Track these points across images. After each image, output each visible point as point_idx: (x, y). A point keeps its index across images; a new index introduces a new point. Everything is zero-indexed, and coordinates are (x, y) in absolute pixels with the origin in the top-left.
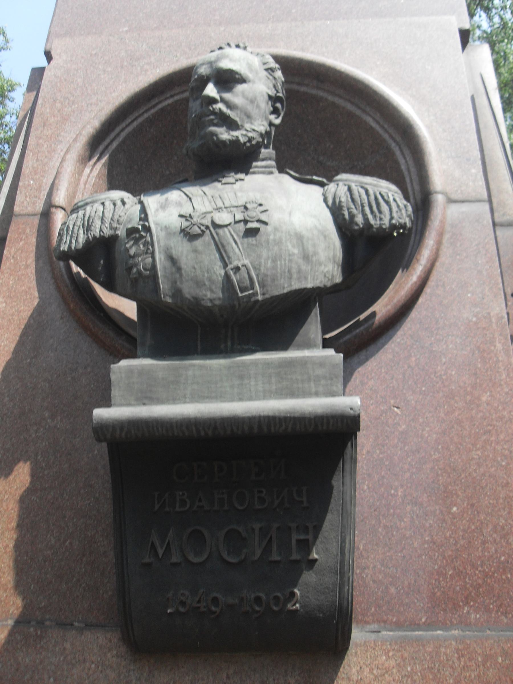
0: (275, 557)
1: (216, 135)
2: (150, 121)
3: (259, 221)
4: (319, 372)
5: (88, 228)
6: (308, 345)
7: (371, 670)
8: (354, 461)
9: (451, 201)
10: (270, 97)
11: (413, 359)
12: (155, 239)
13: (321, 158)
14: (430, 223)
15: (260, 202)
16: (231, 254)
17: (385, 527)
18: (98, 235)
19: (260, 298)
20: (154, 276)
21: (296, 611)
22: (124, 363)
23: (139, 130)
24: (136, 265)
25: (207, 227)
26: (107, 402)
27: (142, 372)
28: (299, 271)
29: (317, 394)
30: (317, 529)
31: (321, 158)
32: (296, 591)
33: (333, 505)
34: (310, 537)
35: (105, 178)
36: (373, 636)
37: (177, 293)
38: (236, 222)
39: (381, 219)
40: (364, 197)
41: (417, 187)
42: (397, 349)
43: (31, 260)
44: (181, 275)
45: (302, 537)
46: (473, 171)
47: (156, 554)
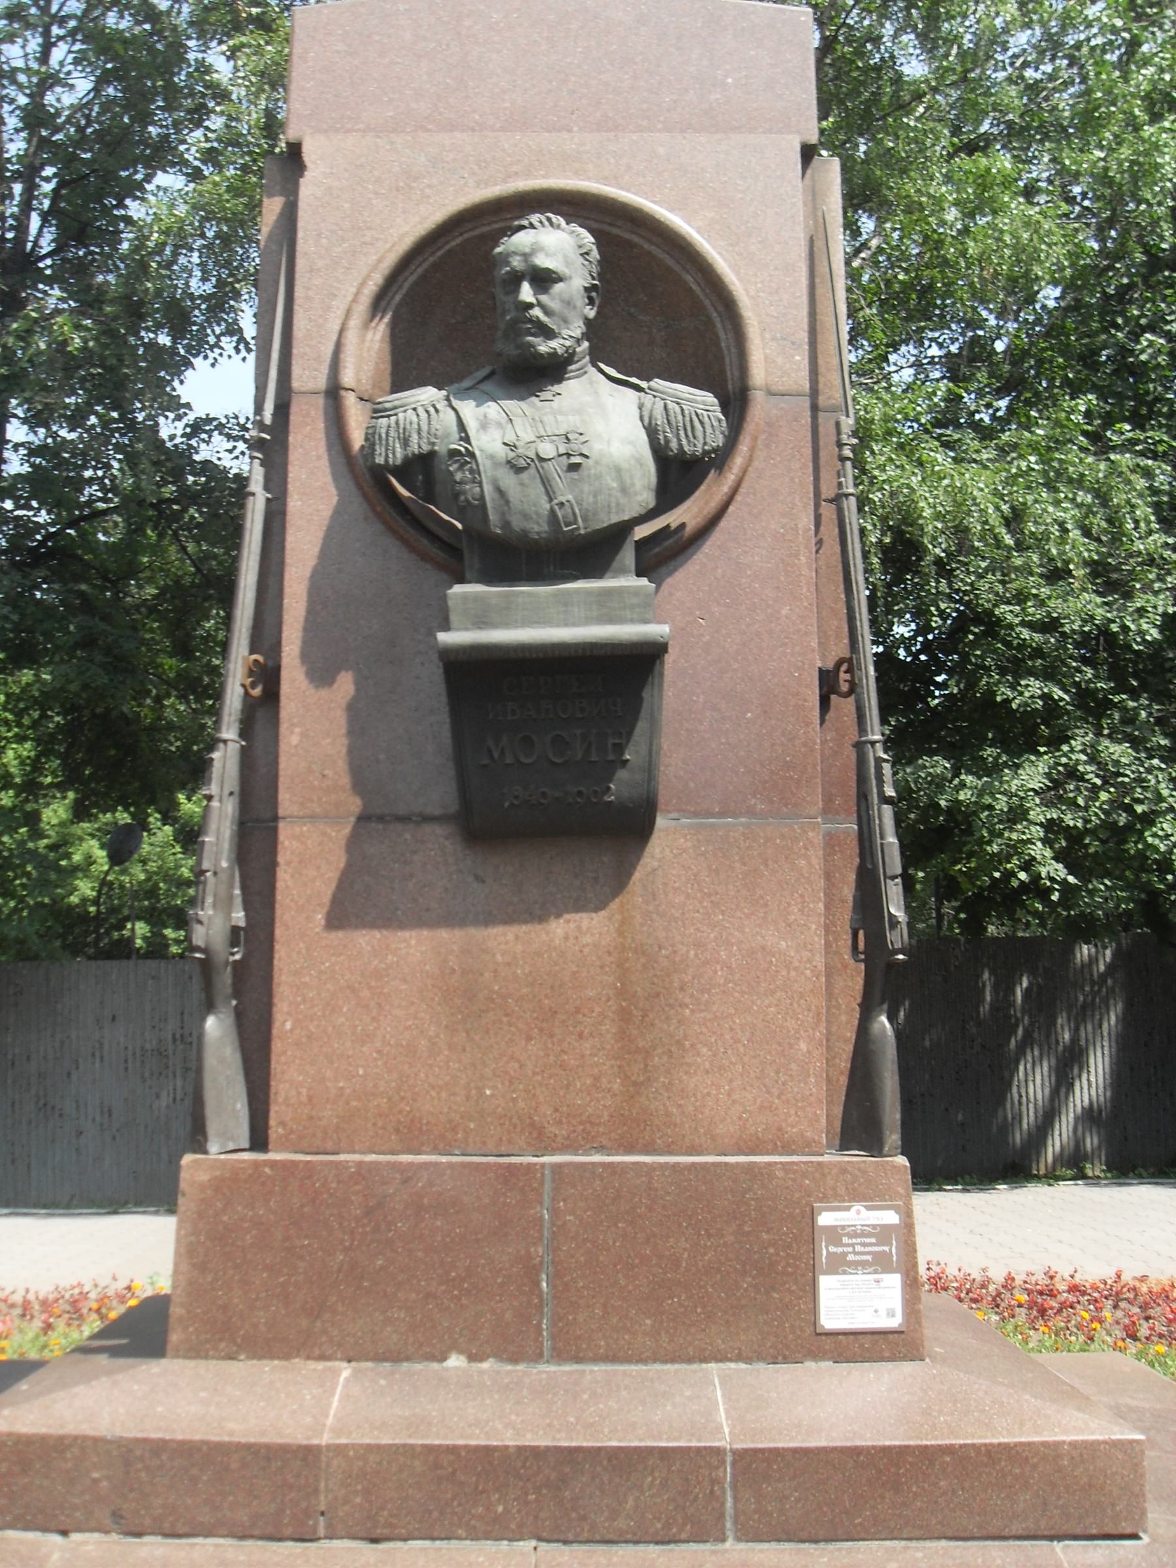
0: (594, 758)
1: (533, 347)
2: (436, 266)
3: (582, 455)
4: (635, 601)
5: (406, 443)
6: (623, 571)
7: (671, 851)
8: (662, 675)
9: (771, 393)
10: (586, 289)
11: (720, 571)
12: (481, 468)
13: (632, 310)
14: (745, 425)
15: (580, 431)
16: (556, 489)
17: (687, 729)
18: (416, 452)
19: (582, 532)
20: (483, 506)
21: (611, 802)
22: (458, 589)
23: (424, 277)
24: (464, 492)
25: (533, 460)
26: (446, 627)
27: (476, 598)
28: (618, 504)
29: (632, 621)
30: (630, 733)
31: (632, 310)
32: (612, 786)
33: (644, 713)
34: (623, 741)
35: (388, 339)
36: (674, 822)
37: (506, 525)
38: (560, 456)
39: (695, 446)
40: (680, 417)
41: (736, 374)
42: (704, 560)
43: (322, 450)
44: (509, 508)
45: (617, 741)
46: (797, 358)
47: (492, 757)
